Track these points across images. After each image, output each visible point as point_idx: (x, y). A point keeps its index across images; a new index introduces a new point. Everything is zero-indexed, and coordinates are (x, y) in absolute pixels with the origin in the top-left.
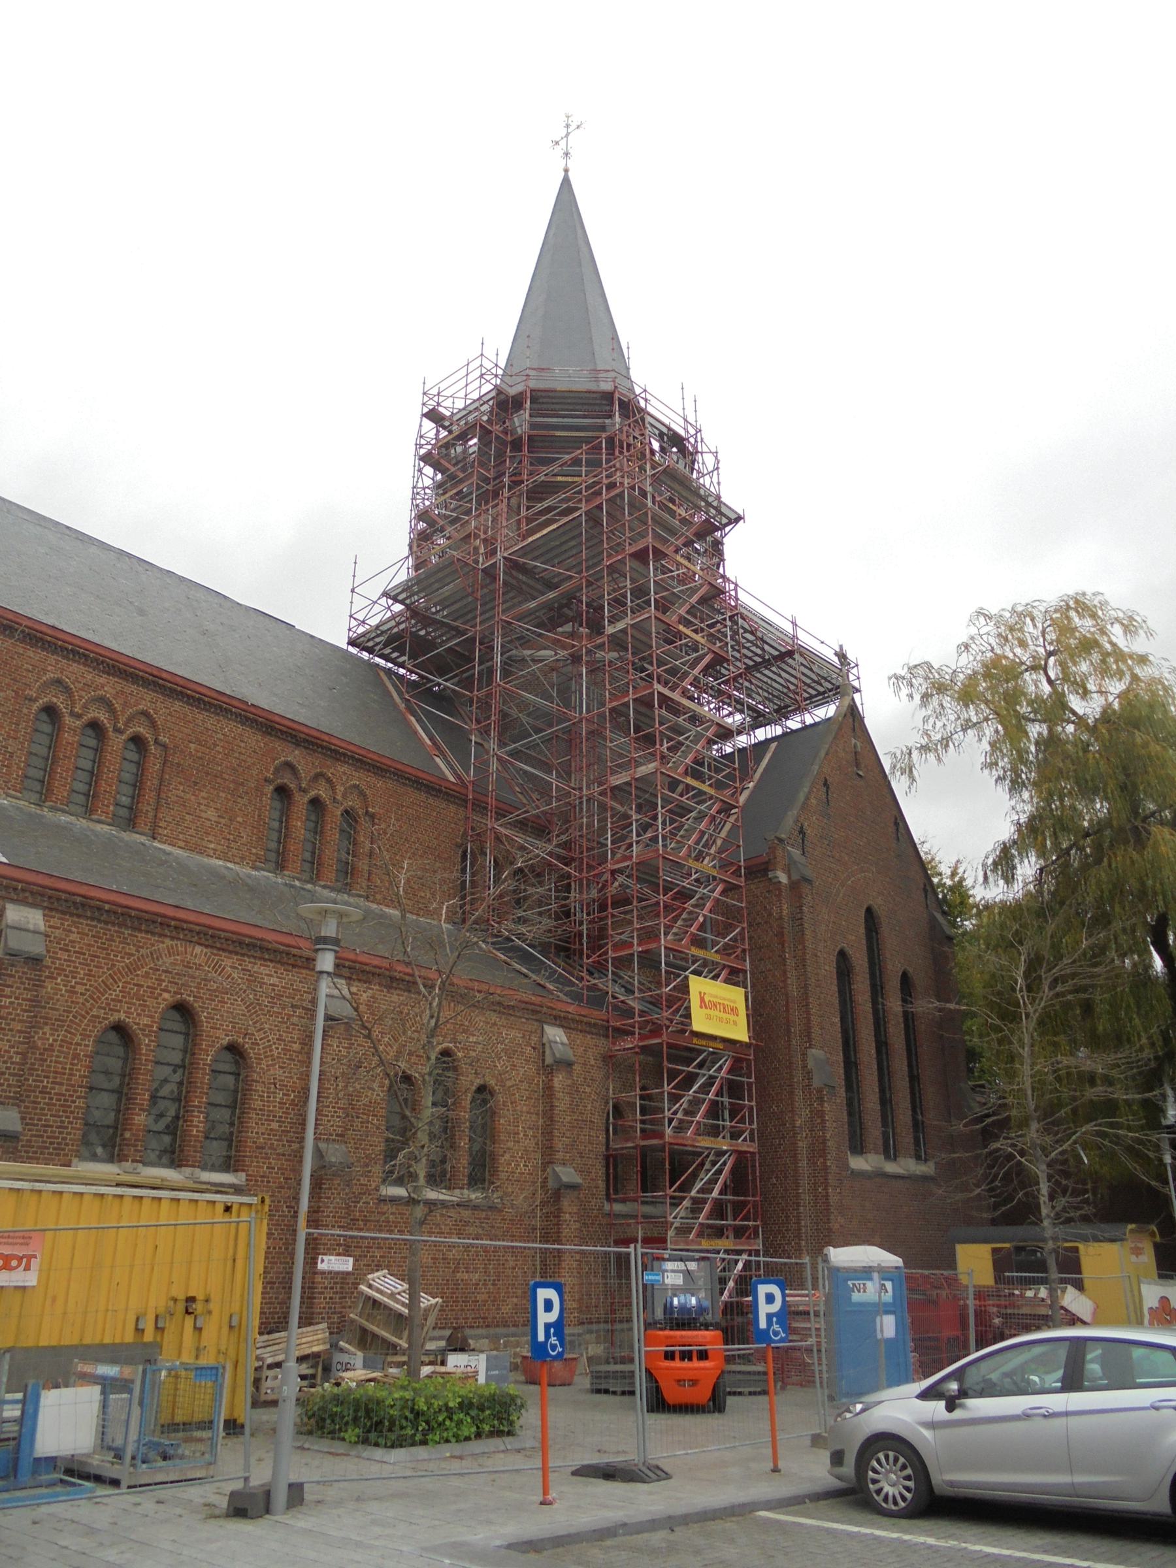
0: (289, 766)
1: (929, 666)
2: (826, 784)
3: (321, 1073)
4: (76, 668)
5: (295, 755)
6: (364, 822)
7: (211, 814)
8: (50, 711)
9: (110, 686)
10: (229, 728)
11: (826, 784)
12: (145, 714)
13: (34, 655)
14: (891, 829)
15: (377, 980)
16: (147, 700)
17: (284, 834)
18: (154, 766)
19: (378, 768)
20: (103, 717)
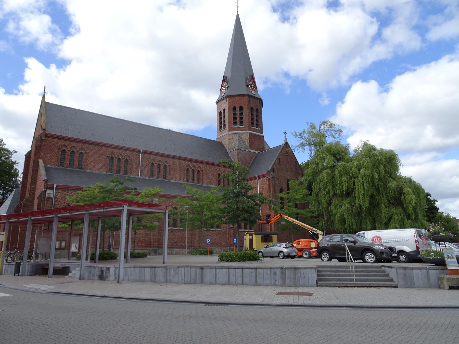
0: (160, 161)
1: (31, 4)
2: (279, 159)
3: (169, 223)
4: (155, 156)
5: (189, 163)
6: (201, 172)
7: (177, 175)
8: (152, 163)
9: (160, 158)
10: (179, 161)
11: (279, 159)
12: (64, 145)
13: (149, 156)
14: (295, 164)
15: (221, 198)
16: (166, 159)
17: (188, 176)
18: (168, 169)
19: (203, 162)
20: (160, 163)
